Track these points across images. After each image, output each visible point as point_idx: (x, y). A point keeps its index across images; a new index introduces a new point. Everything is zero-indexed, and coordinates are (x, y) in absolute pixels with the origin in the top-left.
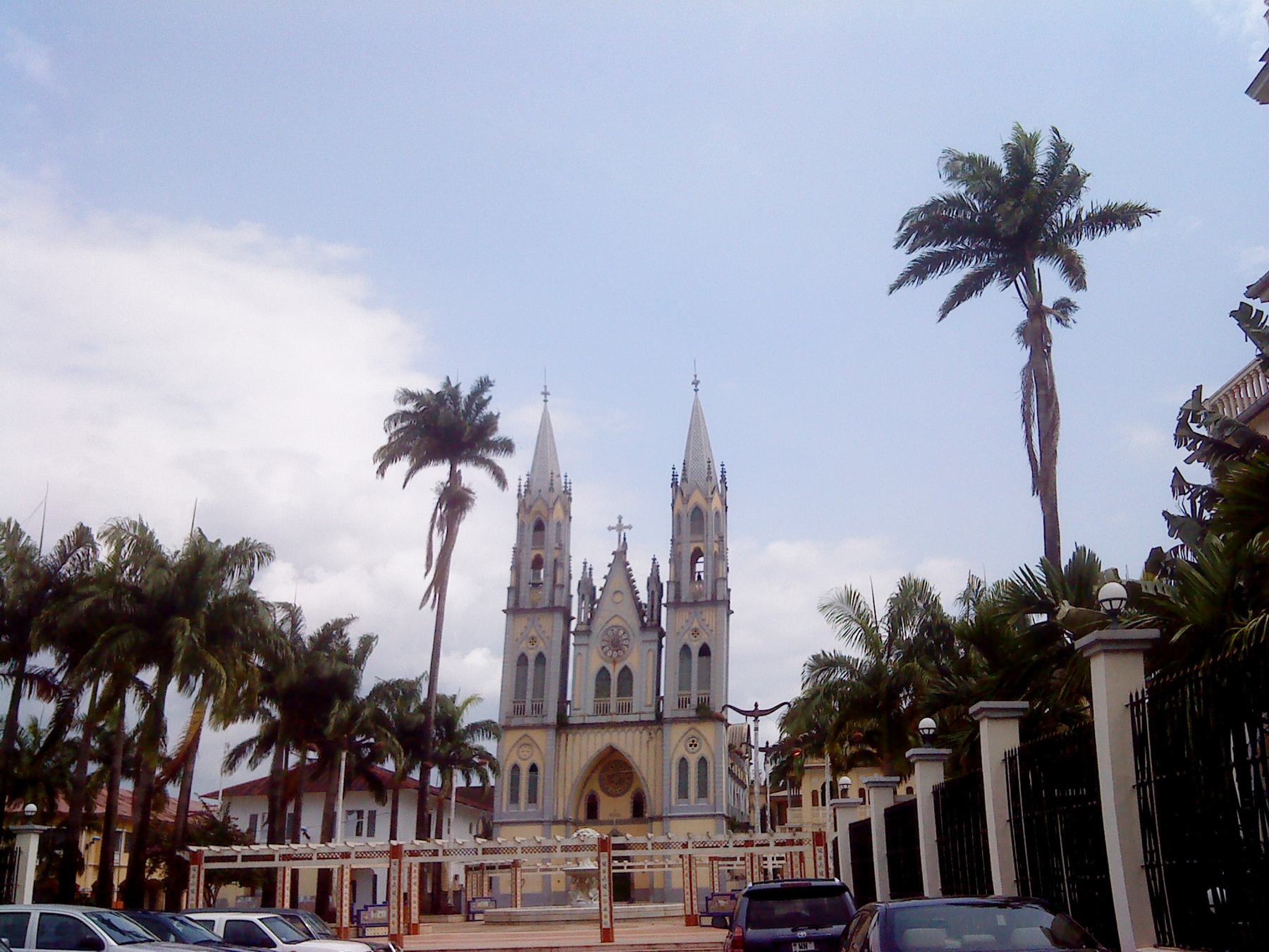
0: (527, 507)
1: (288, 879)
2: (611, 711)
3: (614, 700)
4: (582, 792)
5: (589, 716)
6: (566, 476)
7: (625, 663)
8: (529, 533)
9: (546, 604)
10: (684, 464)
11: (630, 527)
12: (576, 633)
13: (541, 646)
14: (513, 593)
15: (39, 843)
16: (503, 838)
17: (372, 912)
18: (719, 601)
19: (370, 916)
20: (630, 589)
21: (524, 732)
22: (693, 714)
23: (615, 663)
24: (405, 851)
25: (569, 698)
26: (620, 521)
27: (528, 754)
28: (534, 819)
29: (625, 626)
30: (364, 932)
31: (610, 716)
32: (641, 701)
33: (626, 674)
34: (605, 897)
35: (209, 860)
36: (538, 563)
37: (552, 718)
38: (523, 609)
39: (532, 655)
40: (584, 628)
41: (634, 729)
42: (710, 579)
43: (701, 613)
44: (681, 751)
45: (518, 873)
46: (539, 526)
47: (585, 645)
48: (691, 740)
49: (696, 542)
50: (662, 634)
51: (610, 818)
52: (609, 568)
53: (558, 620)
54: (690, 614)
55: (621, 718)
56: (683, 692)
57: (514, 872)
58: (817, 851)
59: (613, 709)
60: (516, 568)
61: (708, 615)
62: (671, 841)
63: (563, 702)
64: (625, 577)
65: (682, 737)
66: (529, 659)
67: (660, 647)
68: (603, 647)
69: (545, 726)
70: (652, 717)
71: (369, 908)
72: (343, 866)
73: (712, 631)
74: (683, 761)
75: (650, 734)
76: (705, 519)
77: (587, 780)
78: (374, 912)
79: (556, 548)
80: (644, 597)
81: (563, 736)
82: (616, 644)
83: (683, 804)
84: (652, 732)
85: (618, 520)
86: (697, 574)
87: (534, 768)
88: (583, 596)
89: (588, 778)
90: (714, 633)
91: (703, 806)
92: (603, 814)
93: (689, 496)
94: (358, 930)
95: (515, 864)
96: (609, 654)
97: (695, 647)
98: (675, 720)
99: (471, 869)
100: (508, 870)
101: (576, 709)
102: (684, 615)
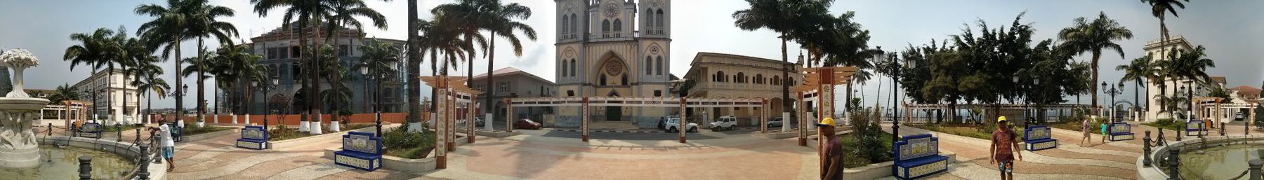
21: (568, 45)
23: (612, 17)
37: (581, 37)
44: (648, 53)
55: (616, 40)
59: (655, 31)
74: (649, 59)
81: (587, 48)
87: (573, 61)
92: (608, 83)
97: (655, 10)
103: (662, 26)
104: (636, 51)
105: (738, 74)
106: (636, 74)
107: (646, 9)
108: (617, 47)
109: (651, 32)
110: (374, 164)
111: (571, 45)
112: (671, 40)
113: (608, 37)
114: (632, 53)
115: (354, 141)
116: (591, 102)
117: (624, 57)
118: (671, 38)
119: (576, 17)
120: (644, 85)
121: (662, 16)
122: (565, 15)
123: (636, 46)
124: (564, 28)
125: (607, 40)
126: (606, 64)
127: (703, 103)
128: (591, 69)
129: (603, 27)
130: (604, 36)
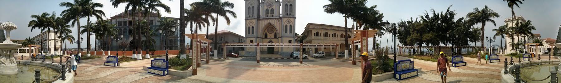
7: (273, 7)
13: (253, 5)
21: (250, 20)
23: (270, 8)
44: (286, 24)
55: (272, 18)
69: (254, 19)
74: (286, 26)
81: (259, 21)
83: (286, 34)
87: (253, 27)
92: (268, 37)
97: (289, 4)
104: (280, 22)
107: (248, 7)
108: (272, 21)
111: (251, 20)
112: (296, 18)
116: (260, 45)
117: (275, 26)
118: (296, 17)
120: (284, 38)
123: (280, 21)
125: (268, 18)
126: (267, 29)
127: (310, 46)
129: (266, 12)
130: (267, 16)
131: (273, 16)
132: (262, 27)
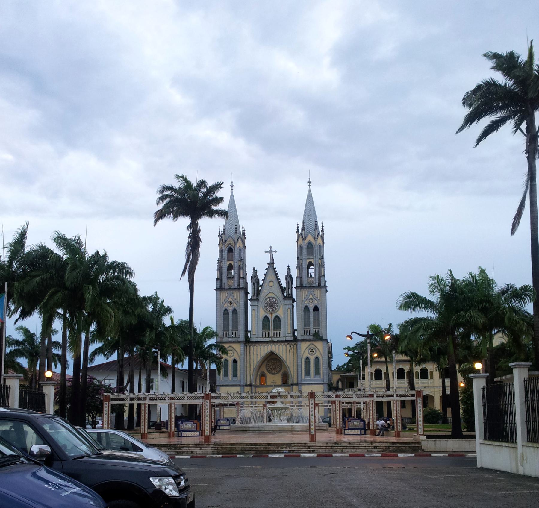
0: (224, 241)
1: (147, 409)
2: (271, 336)
3: (272, 331)
4: (258, 372)
5: (260, 338)
6: (243, 227)
7: (277, 314)
8: (225, 254)
9: (236, 286)
10: (303, 222)
11: (276, 252)
12: (251, 300)
13: (235, 306)
14: (219, 281)
15: (457, 381)
16: (223, 391)
17: (185, 425)
18: (322, 286)
19: (184, 427)
20: (277, 280)
22: (311, 337)
23: (271, 314)
24: (212, 397)
25: (249, 329)
26: (271, 249)
27: (232, 355)
28: (230, 384)
29: (275, 297)
30: (182, 434)
31: (270, 338)
32: (285, 332)
33: (277, 319)
34: (312, 420)
35: (113, 399)
36: (230, 267)
37: (242, 338)
38: (225, 289)
39: (230, 310)
40: (255, 298)
41: (283, 344)
42: (317, 277)
43: (314, 291)
44: (307, 354)
45: (239, 408)
46: (230, 250)
47: (256, 305)
48: (311, 349)
49: (309, 259)
50: (294, 301)
51: (272, 384)
52: (266, 271)
53: (242, 293)
54: (308, 292)
55: (276, 339)
56: (306, 328)
57: (237, 407)
58: (418, 400)
59: (272, 335)
60: (220, 269)
61: (317, 293)
62: (157, 397)
63: (247, 331)
64: (275, 275)
65: (307, 348)
66: (229, 311)
67: (293, 307)
68: (265, 307)
69: (239, 342)
70: (292, 339)
71: (183, 423)
72: (171, 403)
73: (319, 300)
74: (308, 359)
75: (291, 346)
76: (314, 248)
77: (260, 366)
78: (186, 425)
79: (239, 261)
80: (284, 284)
81: (248, 347)
82: (271, 305)
83: (308, 378)
84: (291, 345)
85: (270, 248)
86: (309, 274)
87: (235, 361)
88: (254, 283)
89: (260, 366)
90: (320, 301)
91: (318, 379)
93: (306, 237)
94: (178, 433)
95: (238, 404)
96: (269, 310)
97: (311, 307)
98: (303, 340)
99: (214, 406)
100: (234, 406)
101: (253, 335)
102: (305, 293)
103: (319, 326)
104: (295, 351)
105: (421, 370)
106: (296, 375)
107: (224, 309)
109: (268, 335)
110: (363, 432)
113: (268, 335)
114: (291, 353)
115: (221, 422)
119: (237, 313)
120: (303, 386)
121: (318, 314)
122: (226, 310)
123: (295, 346)
124: (224, 324)
126: (266, 362)
128: (252, 370)
129: (263, 324)
130: (265, 335)
131: (278, 335)
132: (259, 356)
